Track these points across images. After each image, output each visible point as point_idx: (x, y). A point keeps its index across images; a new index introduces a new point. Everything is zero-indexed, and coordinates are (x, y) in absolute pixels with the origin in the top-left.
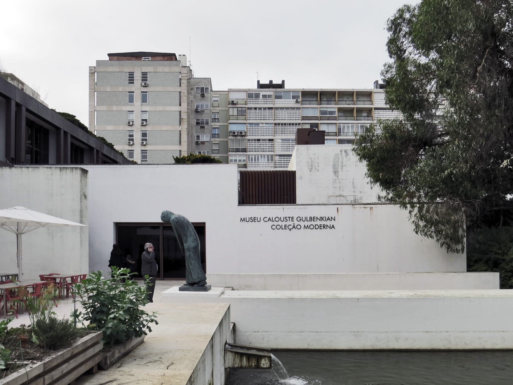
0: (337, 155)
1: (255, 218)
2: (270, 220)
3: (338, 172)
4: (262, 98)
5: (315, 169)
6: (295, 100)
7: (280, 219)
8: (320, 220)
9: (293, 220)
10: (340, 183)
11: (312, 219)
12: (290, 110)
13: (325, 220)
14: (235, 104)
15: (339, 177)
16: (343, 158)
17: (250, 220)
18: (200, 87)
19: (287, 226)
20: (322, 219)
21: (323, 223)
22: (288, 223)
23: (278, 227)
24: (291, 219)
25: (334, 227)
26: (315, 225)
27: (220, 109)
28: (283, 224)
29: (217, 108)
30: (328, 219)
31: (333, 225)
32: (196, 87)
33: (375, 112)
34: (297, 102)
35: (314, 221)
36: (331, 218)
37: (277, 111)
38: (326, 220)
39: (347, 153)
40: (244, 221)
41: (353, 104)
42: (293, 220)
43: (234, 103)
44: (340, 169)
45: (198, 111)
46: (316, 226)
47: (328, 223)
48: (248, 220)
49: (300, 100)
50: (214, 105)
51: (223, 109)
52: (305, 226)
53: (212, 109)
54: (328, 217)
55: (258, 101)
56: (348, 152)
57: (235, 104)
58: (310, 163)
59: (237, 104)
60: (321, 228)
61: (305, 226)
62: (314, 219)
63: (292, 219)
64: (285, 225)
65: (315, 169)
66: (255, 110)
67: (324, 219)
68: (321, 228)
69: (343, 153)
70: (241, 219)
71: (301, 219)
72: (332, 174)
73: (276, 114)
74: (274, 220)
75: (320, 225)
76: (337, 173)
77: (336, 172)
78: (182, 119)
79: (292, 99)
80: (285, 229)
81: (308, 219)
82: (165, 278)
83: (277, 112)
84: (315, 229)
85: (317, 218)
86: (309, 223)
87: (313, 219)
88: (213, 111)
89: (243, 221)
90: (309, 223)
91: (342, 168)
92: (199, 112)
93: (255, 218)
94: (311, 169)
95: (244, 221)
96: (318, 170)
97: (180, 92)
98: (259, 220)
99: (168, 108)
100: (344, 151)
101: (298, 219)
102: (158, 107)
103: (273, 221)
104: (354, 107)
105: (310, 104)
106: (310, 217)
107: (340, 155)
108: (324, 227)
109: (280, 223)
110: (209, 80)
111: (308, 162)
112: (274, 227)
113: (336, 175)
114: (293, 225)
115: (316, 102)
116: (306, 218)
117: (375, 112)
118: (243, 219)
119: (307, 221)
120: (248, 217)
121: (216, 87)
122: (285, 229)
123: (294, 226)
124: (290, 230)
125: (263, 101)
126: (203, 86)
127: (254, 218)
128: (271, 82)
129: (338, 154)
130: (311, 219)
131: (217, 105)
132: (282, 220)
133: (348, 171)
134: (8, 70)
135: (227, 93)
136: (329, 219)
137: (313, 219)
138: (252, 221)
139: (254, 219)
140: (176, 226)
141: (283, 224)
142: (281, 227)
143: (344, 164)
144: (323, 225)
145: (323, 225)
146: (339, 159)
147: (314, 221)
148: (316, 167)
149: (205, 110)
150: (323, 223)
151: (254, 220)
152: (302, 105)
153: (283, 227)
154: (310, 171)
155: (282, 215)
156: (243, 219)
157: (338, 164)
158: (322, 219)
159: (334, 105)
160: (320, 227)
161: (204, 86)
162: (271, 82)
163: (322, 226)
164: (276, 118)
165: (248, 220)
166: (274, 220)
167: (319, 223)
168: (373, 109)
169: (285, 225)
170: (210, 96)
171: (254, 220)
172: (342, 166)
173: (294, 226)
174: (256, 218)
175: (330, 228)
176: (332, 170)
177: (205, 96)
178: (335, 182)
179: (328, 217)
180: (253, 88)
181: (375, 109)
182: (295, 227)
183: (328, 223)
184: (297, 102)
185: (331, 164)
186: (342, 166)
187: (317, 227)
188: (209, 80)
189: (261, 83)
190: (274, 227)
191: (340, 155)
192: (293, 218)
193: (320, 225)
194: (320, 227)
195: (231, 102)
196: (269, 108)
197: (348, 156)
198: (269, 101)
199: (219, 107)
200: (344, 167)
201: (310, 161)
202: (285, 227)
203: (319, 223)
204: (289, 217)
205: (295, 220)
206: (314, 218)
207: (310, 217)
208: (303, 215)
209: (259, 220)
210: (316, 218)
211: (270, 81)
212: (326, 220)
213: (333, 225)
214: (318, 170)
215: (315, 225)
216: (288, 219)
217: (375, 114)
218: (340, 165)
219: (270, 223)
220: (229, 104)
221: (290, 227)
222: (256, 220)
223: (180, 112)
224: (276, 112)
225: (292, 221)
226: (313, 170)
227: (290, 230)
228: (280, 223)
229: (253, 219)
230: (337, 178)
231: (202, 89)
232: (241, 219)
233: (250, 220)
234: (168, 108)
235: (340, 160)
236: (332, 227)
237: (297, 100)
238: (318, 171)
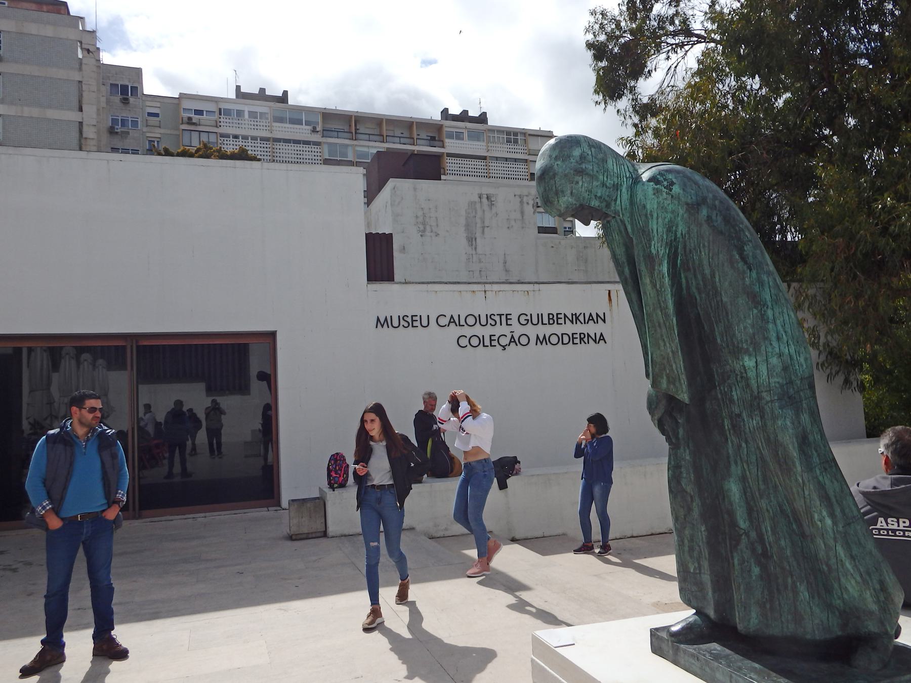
0: (472, 204)
1: (414, 318)
2: (454, 322)
3: (476, 239)
4: (249, 117)
5: (432, 231)
6: (310, 128)
7: (477, 319)
8: (572, 322)
9: (509, 322)
10: (480, 261)
11: (554, 319)
12: (301, 145)
13: (583, 321)
14: (194, 124)
15: (479, 250)
16: (484, 211)
17: (402, 322)
18: (120, 83)
19: (496, 338)
20: (575, 319)
21: (579, 328)
22: (498, 330)
23: (475, 341)
24: (504, 318)
25: (604, 339)
26: (562, 334)
27: (162, 131)
28: (487, 332)
29: (158, 130)
30: (589, 319)
31: (602, 335)
32: (111, 82)
33: (448, 161)
34: (314, 131)
35: (558, 323)
36: (597, 315)
37: (278, 146)
38: (586, 322)
39: (492, 201)
40: (385, 325)
41: (411, 144)
42: (509, 322)
43: (194, 121)
44: (478, 235)
45: (116, 131)
46: (564, 335)
47: (591, 329)
48: (396, 323)
49: (319, 128)
50: (150, 123)
51: (169, 132)
52: (538, 337)
53: (145, 129)
54: (591, 315)
55: (240, 122)
56: (492, 199)
57: (194, 124)
58: (420, 219)
59: (199, 125)
60: (575, 341)
61: (538, 337)
62: (558, 318)
63: (507, 319)
64: (491, 336)
65: (432, 231)
66: (234, 140)
67: (581, 318)
68: (575, 341)
69: (484, 200)
70: (378, 319)
71: (528, 320)
72: (464, 242)
73: (275, 151)
74: (462, 322)
75: (573, 334)
76: (474, 242)
77: (472, 239)
78: (86, 138)
79: (306, 125)
80: (491, 346)
81: (546, 320)
82: (145, 512)
83: (278, 147)
84: (563, 344)
85: (565, 316)
86: (547, 330)
87: (555, 318)
88: (148, 135)
89: (382, 326)
90: (547, 330)
91: (483, 232)
92: (117, 133)
93: (414, 318)
94: (424, 231)
95: (385, 325)
96: (437, 235)
97: (80, 82)
98: (425, 323)
99: (52, 114)
100: (486, 196)
101: (522, 319)
102: (26, 109)
103: (460, 325)
104: (414, 149)
105: (338, 138)
106: (549, 314)
107: (478, 206)
108: (581, 339)
109: (478, 330)
110: (138, 72)
111: (417, 217)
112: (463, 342)
113: (472, 245)
114: (509, 336)
115: (349, 135)
116: (540, 317)
117: (448, 161)
118: (382, 321)
119: (543, 324)
120: (396, 313)
121: (151, 86)
122: (491, 346)
123: (512, 337)
124: (504, 347)
125: (250, 123)
126: (126, 83)
127: (412, 316)
128: (262, 90)
129: (476, 202)
130: (552, 319)
131: (157, 124)
132: (483, 322)
133: (495, 238)
134: (80, 682)
135: (176, 101)
136: (593, 319)
137: (555, 318)
138: (406, 325)
139: (413, 321)
140: (681, 228)
141: (487, 332)
142: (481, 341)
143: (486, 224)
144: (580, 334)
145: (580, 334)
146: (476, 213)
147: (558, 323)
148: (433, 228)
149: (130, 131)
150: (579, 328)
151: (411, 322)
152: (324, 138)
153: (487, 342)
154: (421, 236)
155: (482, 310)
156: (382, 321)
157: (476, 223)
158: (577, 318)
159: (380, 143)
160: (572, 338)
161: (127, 83)
162: (262, 90)
163: (578, 336)
164: (275, 159)
165: (396, 323)
166: (462, 322)
167: (569, 328)
168: (445, 155)
169: (491, 336)
170: (141, 104)
171: (411, 322)
172: (483, 227)
173: (512, 337)
174: (418, 318)
175: (595, 341)
176: (465, 235)
177: (131, 102)
178: (471, 260)
179: (591, 315)
180: (230, 97)
181: (449, 155)
182: (515, 341)
183: (591, 329)
184: (314, 131)
185: (463, 221)
186: (483, 227)
187: (566, 339)
188: (138, 72)
189: (242, 90)
190: (463, 342)
191: (478, 206)
192: (509, 317)
193: (573, 334)
194: (573, 338)
195: (185, 120)
196: (262, 139)
197: (494, 208)
198: (261, 124)
199: (160, 127)
200: (486, 229)
201: (420, 213)
202: (491, 340)
203: (569, 328)
204: (500, 315)
205: (514, 321)
206: (559, 316)
207: (549, 314)
208: (533, 310)
209: (425, 323)
210: (562, 316)
211: (260, 88)
212: (586, 322)
213: (602, 335)
214: (437, 235)
215: (562, 334)
216: (497, 318)
217: (448, 164)
218: (479, 225)
219: (455, 331)
220: (182, 123)
221: (504, 341)
222: (417, 324)
223: (81, 123)
224: (275, 147)
225: (507, 324)
226: (428, 233)
227: (504, 347)
228: (478, 330)
229: (409, 320)
230: (474, 252)
231: (124, 89)
232: (378, 319)
233: (402, 322)
234: (52, 114)
235: (479, 213)
236: (600, 339)
237: (314, 128)
238: (436, 236)
